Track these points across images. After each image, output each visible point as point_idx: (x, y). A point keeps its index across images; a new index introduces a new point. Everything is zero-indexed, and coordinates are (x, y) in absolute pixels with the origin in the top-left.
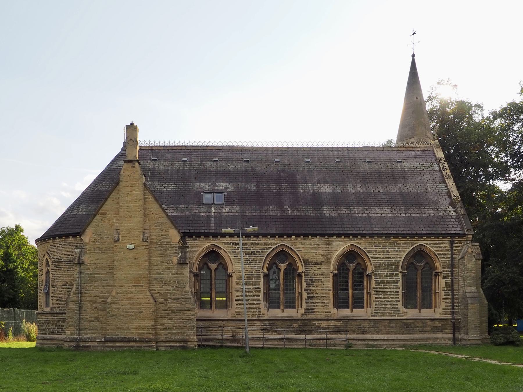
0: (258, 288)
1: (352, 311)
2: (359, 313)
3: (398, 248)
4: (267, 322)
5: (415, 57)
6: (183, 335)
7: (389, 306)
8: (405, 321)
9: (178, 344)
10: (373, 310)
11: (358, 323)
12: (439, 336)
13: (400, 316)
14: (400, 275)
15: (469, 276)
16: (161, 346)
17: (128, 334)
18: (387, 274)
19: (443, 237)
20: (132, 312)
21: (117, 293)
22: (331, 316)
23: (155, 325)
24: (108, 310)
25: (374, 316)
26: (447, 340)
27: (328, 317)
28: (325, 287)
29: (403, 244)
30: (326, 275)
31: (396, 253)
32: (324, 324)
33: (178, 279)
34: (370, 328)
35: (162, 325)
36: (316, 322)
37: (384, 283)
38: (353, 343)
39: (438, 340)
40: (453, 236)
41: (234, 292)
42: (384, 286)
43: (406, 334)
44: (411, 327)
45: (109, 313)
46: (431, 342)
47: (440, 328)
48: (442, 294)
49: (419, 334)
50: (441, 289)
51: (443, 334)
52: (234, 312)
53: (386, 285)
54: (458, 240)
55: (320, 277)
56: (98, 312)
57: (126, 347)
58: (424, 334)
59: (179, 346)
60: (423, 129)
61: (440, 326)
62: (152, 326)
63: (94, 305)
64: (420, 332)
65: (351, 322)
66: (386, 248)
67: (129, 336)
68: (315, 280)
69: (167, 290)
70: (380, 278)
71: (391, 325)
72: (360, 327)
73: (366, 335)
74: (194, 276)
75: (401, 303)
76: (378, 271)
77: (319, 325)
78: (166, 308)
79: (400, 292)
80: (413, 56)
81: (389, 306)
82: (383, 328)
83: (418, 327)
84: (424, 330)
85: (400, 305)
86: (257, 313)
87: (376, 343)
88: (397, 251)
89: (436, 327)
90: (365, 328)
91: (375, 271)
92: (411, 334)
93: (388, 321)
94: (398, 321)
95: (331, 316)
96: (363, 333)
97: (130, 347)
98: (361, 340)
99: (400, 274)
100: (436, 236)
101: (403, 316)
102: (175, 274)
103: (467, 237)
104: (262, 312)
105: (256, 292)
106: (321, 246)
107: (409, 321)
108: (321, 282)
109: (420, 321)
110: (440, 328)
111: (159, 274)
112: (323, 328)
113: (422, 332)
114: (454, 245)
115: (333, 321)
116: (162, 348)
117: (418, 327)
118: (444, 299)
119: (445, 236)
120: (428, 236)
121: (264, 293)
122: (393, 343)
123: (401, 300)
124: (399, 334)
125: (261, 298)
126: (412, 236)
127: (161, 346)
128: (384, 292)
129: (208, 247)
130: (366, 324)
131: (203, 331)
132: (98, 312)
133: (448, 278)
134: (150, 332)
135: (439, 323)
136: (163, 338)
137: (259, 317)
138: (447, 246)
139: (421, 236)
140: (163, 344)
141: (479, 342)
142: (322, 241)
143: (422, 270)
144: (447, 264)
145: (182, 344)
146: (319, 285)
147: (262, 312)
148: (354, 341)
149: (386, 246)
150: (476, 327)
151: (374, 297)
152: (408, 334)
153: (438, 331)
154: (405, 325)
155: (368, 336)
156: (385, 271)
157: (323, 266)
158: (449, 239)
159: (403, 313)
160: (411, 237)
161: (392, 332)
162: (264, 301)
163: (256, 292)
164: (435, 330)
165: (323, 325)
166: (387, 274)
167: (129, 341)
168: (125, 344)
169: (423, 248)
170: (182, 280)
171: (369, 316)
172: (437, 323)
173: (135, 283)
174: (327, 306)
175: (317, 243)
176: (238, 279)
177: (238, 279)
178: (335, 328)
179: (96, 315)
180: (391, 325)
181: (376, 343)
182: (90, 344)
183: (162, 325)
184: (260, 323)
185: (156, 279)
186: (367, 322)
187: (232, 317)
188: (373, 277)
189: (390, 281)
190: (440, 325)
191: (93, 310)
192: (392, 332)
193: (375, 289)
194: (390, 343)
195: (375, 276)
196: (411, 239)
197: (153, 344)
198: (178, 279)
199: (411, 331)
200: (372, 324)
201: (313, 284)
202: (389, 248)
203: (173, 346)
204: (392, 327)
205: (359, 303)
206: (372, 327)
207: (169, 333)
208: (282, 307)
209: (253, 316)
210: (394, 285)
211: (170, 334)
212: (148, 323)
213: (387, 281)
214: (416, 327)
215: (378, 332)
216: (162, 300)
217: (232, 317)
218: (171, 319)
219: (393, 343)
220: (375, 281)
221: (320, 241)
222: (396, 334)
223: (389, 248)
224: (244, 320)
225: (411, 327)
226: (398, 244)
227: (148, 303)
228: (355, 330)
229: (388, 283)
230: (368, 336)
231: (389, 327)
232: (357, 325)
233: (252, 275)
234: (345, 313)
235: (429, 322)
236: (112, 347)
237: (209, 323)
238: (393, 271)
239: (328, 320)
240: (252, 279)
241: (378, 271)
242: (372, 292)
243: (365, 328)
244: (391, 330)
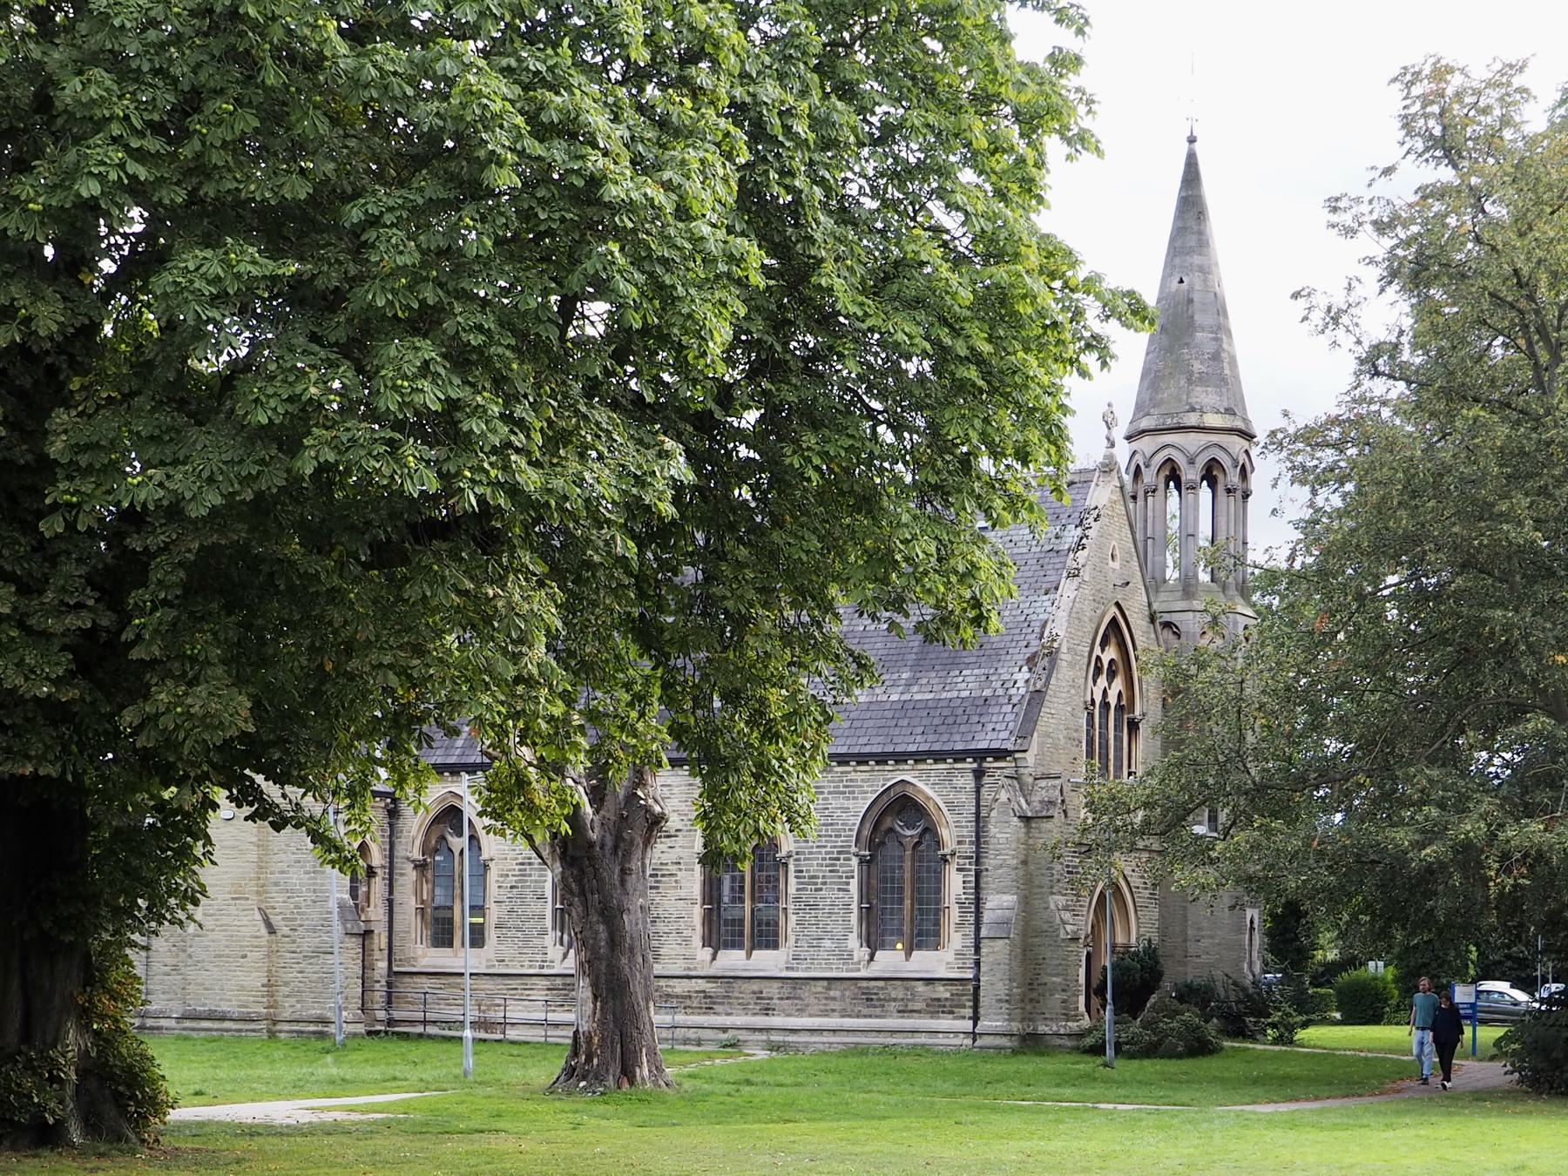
0: (542, 897)
1: (749, 956)
2: (767, 961)
3: (849, 792)
4: (559, 981)
5: (1197, 146)
6: (322, 1008)
7: (827, 943)
8: (864, 984)
9: (312, 1028)
10: (791, 953)
11: (755, 986)
12: (945, 1023)
13: (852, 971)
14: (855, 861)
15: (1001, 866)
16: (280, 1031)
17: (222, 1003)
18: (824, 859)
19: (956, 761)
20: (228, 956)
21: (205, 915)
22: (695, 969)
23: (268, 985)
24: (190, 950)
25: (792, 969)
26: (962, 1036)
27: (689, 969)
28: (683, 894)
29: (863, 780)
30: (686, 864)
31: (846, 804)
32: (680, 987)
33: (315, 884)
34: (782, 999)
35: (286, 984)
36: (662, 982)
37: (816, 884)
38: (741, 1038)
39: (941, 1035)
40: (980, 755)
41: (493, 906)
42: (816, 890)
43: (865, 1016)
44: (879, 1000)
45: (190, 956)
46: (922, 1039)
47: (948, 1004)
48: (955, 912)
49: (898, 1017)
50: (953, 900)
51: (955, 1018)
52: (492, 956)
53: (821, 889)
54: (996, 765)
55: (673, 869)
56: (177, 956)
57: (217, 1030)
58: (909, 1017)
59: (314, 1033)
60: (1182, 382)
61: (947, 999)
62: (263, 986)
63: (172, 939)
64: (899, 1012)
65: (739, 981)
66: (822, 793)
67: (224, 1007)
68: (663, 876)
69: (296, 907)
70: (808, 871)
71: (832, 993)
72: (759, 996)
73: (773, 1018)
74: (416, 867)
75: (855, 935)
76: (804, 853)
77: (669, 990)
78: (293, 947)
79: (855, 906)
80: (1192, 140)
81: (827, 943)
82: (812, 1000)
83: (895, 1000)
84: (910, 1008)
85: (853, 942)
86: (539, 957)
87: (791, 1038)
88: (848, 799)
89: (938, 1000)
90: (771, 999)
91: (797, 853)
92: (877, 1017)
93: (825, 983)
94: (848, 982)
95: (695, 969)
96: (767, 1011)
97: (222, 1030)
98: (761, 1030)
99: (854, 859)
100: (939, 757)
101: (859, 970)
102: (309, 873)
103: (1015, 759)
104: (549, 957)
105: (535, 907)
106: (676, 790)
107: (873, 983)
108: (676, 882)
109: (899, 983)
110: (948, 1004)
111: (283, 872)
112: (677, 997)
113: (903, 1012)
114: (986, 780)
115: (700, 981)
116: (282, 1035)
117: (895, 1000)
118: (960, 925)
119: (959, 756)
120: (920, 757)
121: (555, 911)
122: (832, 1039)
123: (855, 930)
124: (850, 1016)
125: (548, 923)
126: (881, 759)
127: (280, 1031)
128: (814, 907)
129: (442, 799)
130: (773, 989)
131: (429, 1001)
132: (177, 956)
133: (970, 870)
134: (260, 999)
135: (946, 990)
136: (286, 1015)
137: (542, 967)
138: (968, 782)
139: (900, 758)
140: (286, 1027)
141: (1004, 1042)
142: (679, 779)
143: (914, 848)
144: (968, 831)
145: (320, 1028)
146: (670, 888)
147: (549, 957)
148: (744, 1032)
149: (823, 787)
150: (1000, 1001)
151: (793, 919)
152: (870, 1016)
153: (943, 1012)
154: (863, 994)
155: (777, 1021)
156: (820, 853)
157: (680, 841)
158: (969, 764)
159: (859, 963)
160: (878, 763)
161: (833, 1011)
162: (554, 928)
163: (535, 907)
164: (937, 1008)
165: (678, 990)
166: (824, 859)
167: (223, 1018)
168: (216, 1025)
169: (910, 792)
170: (323, 885)
171: (781, 970)
172: (942, 989)
173: (235, 892)
174: (687, 940)
175: (669, 782)
176: (502, 876)
177: (502, 876)
178: (705, 997)
179: (174, 961)
180: (832, 993)
181: (791, 1038)
182: (163, 1023)
183: (286, 984)
184: (545, 983)
185: (276, 884)
186: (776, 984)
187: (488, 967)
188: (792, 868)
189: (832, 877)
190: (948, 995)
191: (170, 951)
192: (833, 1011)
193: (797, 900)
194: (825, 1040)
195: (796, 866)
196: (881, 767)
197: (263, 1025)
198: (315, 884)
199: (878, 1011)
200: (786, 991)
201: (657, 888)
202: (829, 793)
203: (302, 1032)
204: (834, 999)
205: (767, 936)
206: (788, 998)
207: (298, 1002)
208: (747, 943)
209: (531, 967)
210: (839, 890)
211: (299, 1006)
212: (256, 980)
213: (824, 877)
214: (889, 1000)
215: (801, 1011)
216: (286, 930)
217: (488, 967)
218: (301, 972)
219: (832, 1039)
220: (797, 877)
221: (673, 778)
222: (843, 1016)
223: (829, 793)
224: (462, 974)
225: (879, 1000)
226: (851, 780)
227: (257, 937)
228: (749, 1004)
229: (825, 883)
230: (777, 1021)
231: (826, 999)
232: (754, 993)
233: (530, 864)
234: (732, 960)
235: (920, 987)
236: (193, 1029)
237: (444, 980)
238: (839, 853)
239: (689, 977)
240: (530, 875)
241: (804, 853)
242: (791, 907)
243: (771, 999)
244: (832, 1005)
